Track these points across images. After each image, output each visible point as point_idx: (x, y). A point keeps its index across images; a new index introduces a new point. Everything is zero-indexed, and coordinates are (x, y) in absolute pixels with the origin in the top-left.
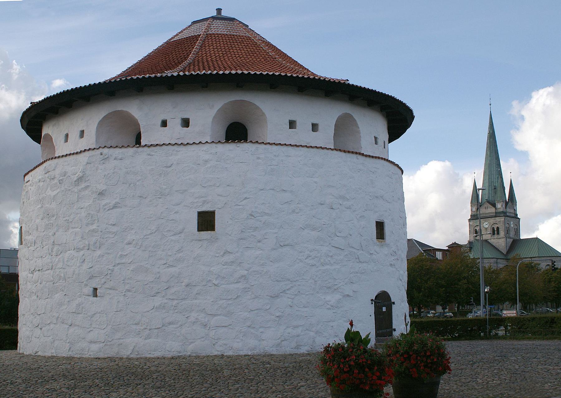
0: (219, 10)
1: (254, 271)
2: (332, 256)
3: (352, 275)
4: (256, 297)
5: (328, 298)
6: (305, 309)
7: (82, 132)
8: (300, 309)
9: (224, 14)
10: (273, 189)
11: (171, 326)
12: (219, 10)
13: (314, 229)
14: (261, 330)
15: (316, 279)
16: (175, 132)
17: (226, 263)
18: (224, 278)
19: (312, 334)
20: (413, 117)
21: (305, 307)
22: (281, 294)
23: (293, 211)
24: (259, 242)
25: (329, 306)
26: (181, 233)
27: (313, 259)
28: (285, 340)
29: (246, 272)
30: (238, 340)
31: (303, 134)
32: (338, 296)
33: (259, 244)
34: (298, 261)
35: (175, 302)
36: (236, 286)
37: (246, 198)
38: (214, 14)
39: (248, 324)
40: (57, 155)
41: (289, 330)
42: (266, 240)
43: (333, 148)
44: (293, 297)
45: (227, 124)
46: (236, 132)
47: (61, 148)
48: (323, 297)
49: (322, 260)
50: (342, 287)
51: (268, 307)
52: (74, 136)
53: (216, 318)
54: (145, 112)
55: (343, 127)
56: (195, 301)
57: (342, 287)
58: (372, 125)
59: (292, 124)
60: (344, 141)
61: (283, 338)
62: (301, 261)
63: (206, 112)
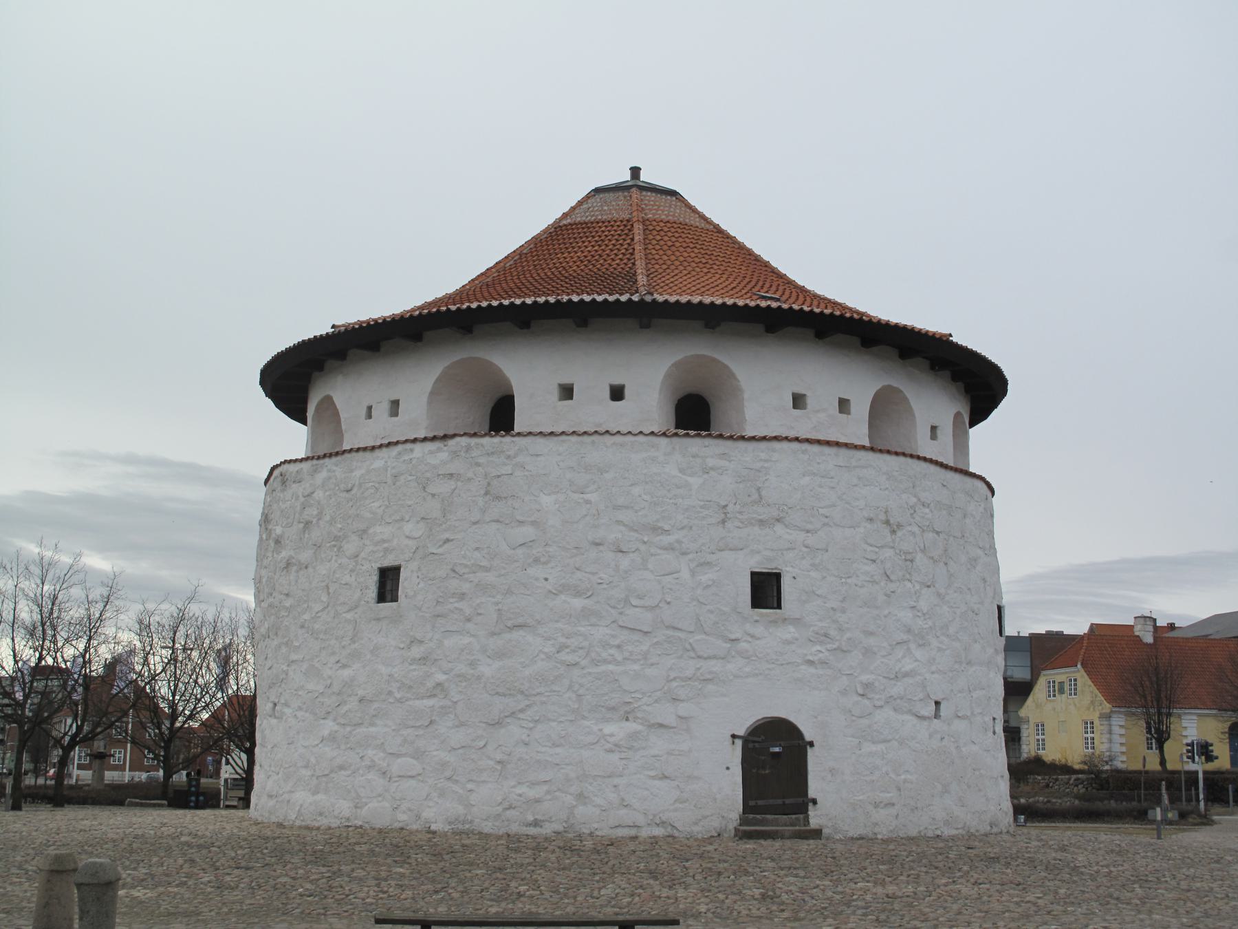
0: (635, 171)
1: (459, 676)
2: (619, 647)
3: (674, 684)
4: (462, 724)
5: (609, 729)
6: (558, 750)
7: (395, 404)
8: (544, 749)
9: (644, 177)
10: (498, 521)
11: (343, 772)
12: (635, 171)
13: (578, 594)
14: (470, 786)
15: (581, 692)
16: (592, 407)
17: (414, 661)
18: (410, 687)
19: (569, 799)
20: (1004, 393)
21: (555, 745)
22: (508, 720)
23: (537, 560)
24: (469, 620)
25: (608, 746)
26: (356, 607)
27: (574, 651)
28: (510, 807)
29: (445, 677)
30: (431, 804)
31: (592, 407)
32: (632, 726)
33: (469, 626)
34: (542, 656)
35: (348, 729)
36: (431, 702)
37: (447, 541)
38: (626, 176)
39: (448, 774)
40: (346, 447)
41: (519, 790)
42: (480, 618)
43: (867, 444)
44: (531, 725)
45: (681, 394)
46: (694, 414)
47: (357, 433)
48: (595, 728)
49: (593, 655)
50: (645, 707)
51: (482, 743)
52: (381, 410)
53: (399, 760)
54: (530, 371)
55: (885, 408)
56: (372, 729)
57: (645, 707)
58: (932, 405)
59: (567, 392)
60: (885, 433)
61: (506, 805)
62: (549, 657)
63: (649, 373)
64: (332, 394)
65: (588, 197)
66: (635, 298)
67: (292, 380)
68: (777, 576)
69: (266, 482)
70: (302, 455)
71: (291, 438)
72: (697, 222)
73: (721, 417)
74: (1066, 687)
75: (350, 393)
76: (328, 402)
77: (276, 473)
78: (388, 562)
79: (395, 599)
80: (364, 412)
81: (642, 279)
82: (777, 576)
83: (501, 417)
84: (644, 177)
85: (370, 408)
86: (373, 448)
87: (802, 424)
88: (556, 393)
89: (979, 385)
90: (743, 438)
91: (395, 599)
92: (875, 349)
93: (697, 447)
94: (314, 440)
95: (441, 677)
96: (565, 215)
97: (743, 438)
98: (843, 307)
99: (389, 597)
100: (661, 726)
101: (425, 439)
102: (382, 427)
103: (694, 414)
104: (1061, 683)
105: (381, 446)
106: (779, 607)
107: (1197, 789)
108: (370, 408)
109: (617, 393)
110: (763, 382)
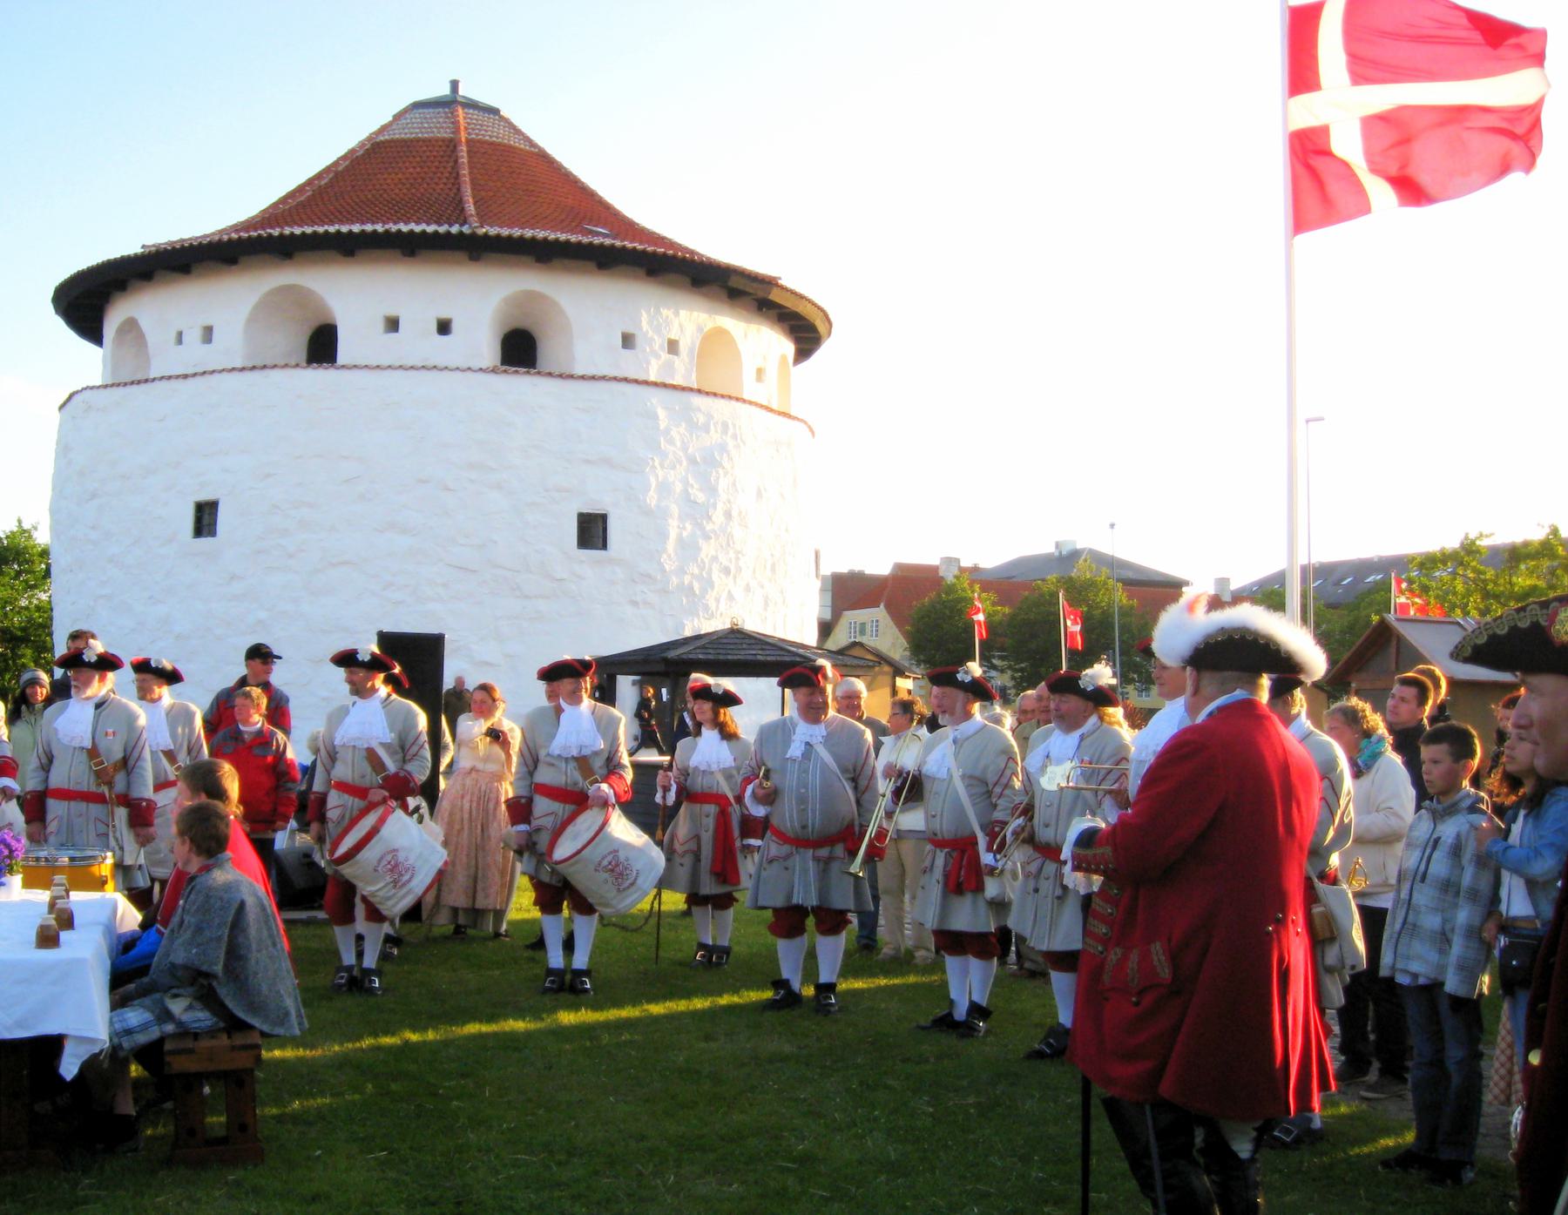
0: (455, 85)
12: (455, 85)
16: (417, 341)
31: (417, 341)
45: (507, 329)
46: (519, 350)
47: (165, 359)
52: (193, 336)
54: (353, 296)
59: (393, 325)
64: (136, 316)
65: (819, 308)
66: (466, 229)
67: (86, 301)
68: (603, 518)
69: (62, 407)
70: (99, 383)
71: (84, 361)
72: (514, 141)
73: (548, 353)
74: (868, 628)
75: (149, 310)
76: (131, 326)
77: (76, 399)
78: (205, 496)
79: (213, 533)
80: (173, 335)
81: (471, 208)
82: (603, 518)
83: (322, 346)
84: (462, 92)
85: (180, 334)
86: (185, 377)
87: (627, 364)
88: (381, 326)
89: (805, 331)
90: (571, 377)
91: (213, 533)
92: (704, 289)
93: (520, 384)
94: (114, 364)
95: (263, 615)
96: (384, 129)
97: (571, 377)
98: (692, 252)
99: (205, 530)
100: (487, 664)
101: (243, 369)
102: (195, 354)
103: (519, 350)
104: (863, 624)
105: (195, 375)
106: (604, 546)
107: (607, 1026)
108: (180, 334)
109: (444, 327)
110: (586, 312)
